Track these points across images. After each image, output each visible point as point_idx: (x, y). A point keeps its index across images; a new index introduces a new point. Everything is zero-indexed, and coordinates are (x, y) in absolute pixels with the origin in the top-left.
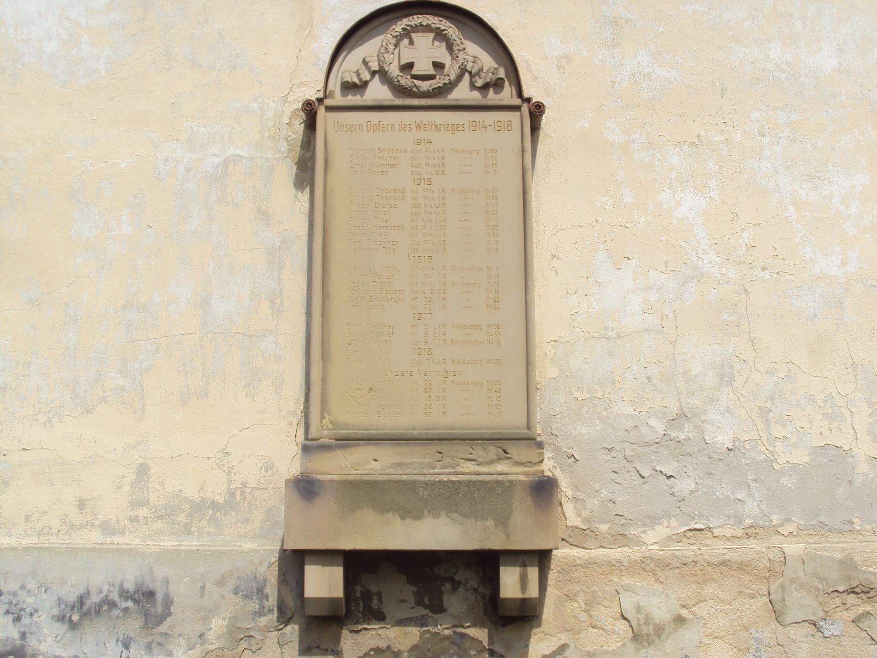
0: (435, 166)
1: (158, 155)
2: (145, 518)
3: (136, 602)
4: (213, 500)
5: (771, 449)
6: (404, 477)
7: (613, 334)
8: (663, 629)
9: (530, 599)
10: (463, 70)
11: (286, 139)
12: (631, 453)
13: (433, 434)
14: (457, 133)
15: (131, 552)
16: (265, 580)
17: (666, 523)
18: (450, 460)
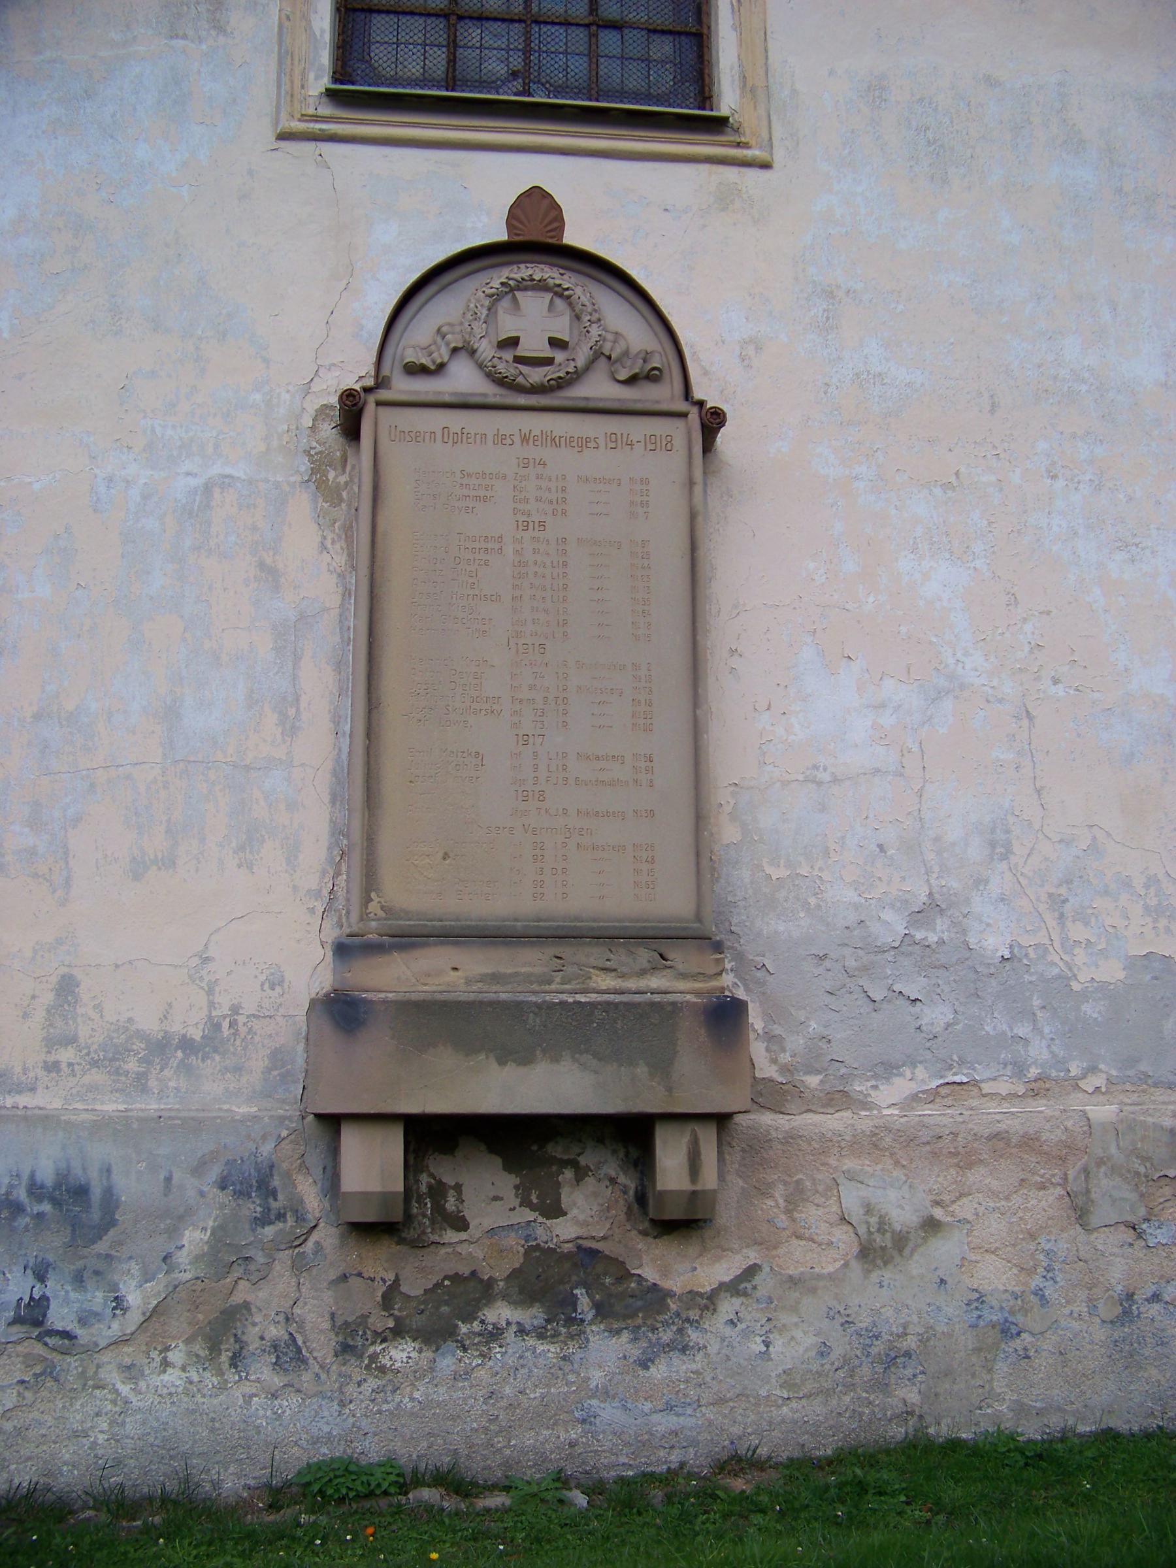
0: (551, 502)
1: (97, 471)
2: (70, 1065)
3: (56, 1202)
4: (184, 1036)
5: (1066, 958)
6: (503, 996)
7: (825, 777)
8: (907, 1239)
9: (704, 1191)
10: (598, 354)
11: (307, 453)
12: (854, 963)
13: (547, 928)
14: (586, 451)
15: (46, 1120)
16: (272, 1167)
17: (908, 1075)
18: (575, 969)
